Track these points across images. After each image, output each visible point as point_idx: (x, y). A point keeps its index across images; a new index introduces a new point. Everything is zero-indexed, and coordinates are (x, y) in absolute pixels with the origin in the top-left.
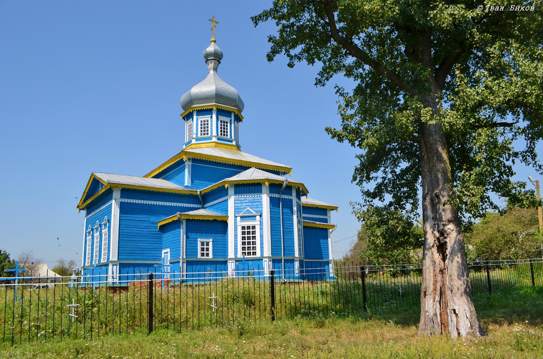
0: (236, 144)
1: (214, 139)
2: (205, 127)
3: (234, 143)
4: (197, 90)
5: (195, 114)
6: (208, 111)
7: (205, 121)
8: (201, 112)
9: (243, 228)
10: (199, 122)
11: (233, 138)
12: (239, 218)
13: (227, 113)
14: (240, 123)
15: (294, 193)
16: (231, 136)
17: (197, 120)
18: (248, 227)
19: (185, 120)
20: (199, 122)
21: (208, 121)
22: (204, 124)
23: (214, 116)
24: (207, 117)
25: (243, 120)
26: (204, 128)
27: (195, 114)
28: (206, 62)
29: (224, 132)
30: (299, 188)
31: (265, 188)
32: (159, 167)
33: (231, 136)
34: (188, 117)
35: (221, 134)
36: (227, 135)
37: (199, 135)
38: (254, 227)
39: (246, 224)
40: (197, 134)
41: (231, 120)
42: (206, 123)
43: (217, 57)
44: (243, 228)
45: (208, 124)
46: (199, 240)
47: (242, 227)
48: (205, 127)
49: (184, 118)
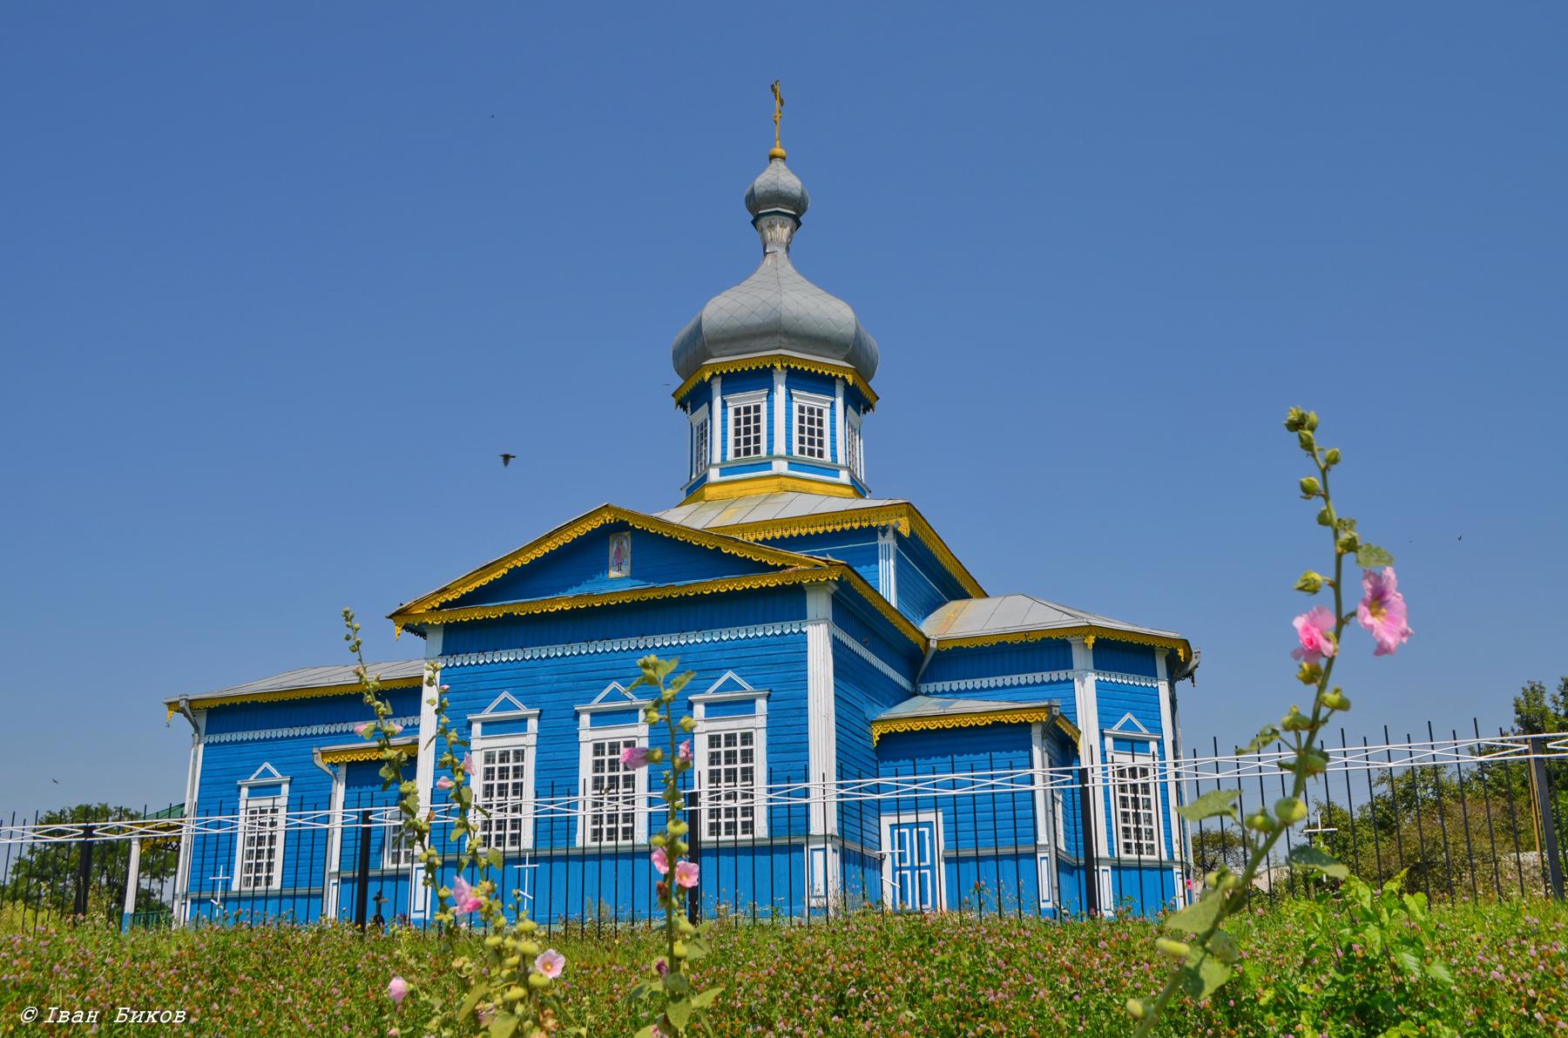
1: (780, 467)
2: (748, 423)
3: (844, 477)
4: (725, 308)
5: (717, 387)
6: (759, 378)
8: (736, 381)
10: (731, 412)
11: (841, 460)
12: (1109, 741)
13: (821, 383)
16: (834, 455)
17: (724, 405)
19: (685, 409)
20: (731, 412)
21: (757, 409)
23: (781, 391)
24: (755, 398)
25: (877, 405)
27: (717, 387)
28: (754, 223)
30: (1174, 652)
31: (1081, 657)
32: (537, 544)
33: (834, 455)
34: (695, 398)
35: (802, 451)
36: (821, 454)
37: (730, 456)
38: (747, 738)
39: (723, 726)
41: (833, 404)
42: (752, 415)
43: (794, 208)
45: (757, 419)
47: (712, 738)
48: (748, 423)
49: (682, 404)
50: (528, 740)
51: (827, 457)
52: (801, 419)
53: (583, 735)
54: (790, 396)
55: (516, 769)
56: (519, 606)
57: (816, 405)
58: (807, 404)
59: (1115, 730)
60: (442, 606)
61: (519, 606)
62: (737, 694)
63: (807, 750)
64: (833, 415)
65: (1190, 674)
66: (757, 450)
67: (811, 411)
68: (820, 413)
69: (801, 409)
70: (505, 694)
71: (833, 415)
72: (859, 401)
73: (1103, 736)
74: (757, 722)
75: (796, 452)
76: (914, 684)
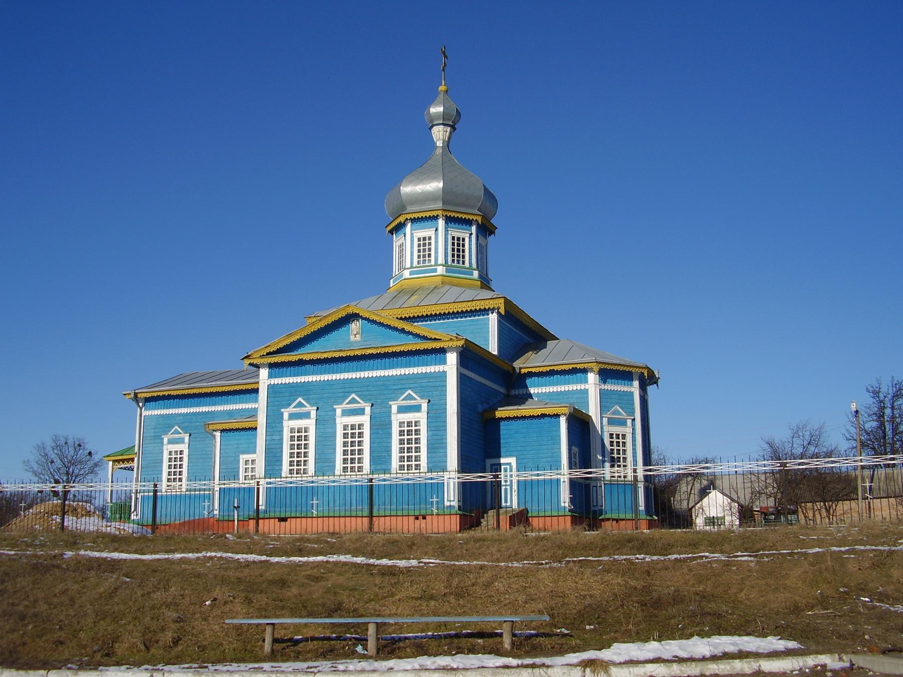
0: (480, 276)
2: (424, 242)
7: (424, 239)
9: (292, 430)
12: (605, 420)
14: (491, 238)
15: (636, 383)
16: (470, 263)
18: (409, 424)
21: (430, 238)
22: (424, 245)
24: (428, 232)
26: (424, 250)
29: (458, 250)
35: (453, 261)
37: (415, 264)
40: (412, 263)
42: (427, 242)
44: (292, 430)
45: (430, 244)
46: (241, 456)
48: (424, 242)
50: (365, 420)
51: (467, 264)
52: (453, 244)
53: (393, 417)
54: (446, 231)
55: (359, 433)
56: (407, 327)
57: (461, 235)
58: (456, 235)
59: (609, 415)
60: (268, 354)
61: (407, 327)
62: (412, 403)
63: (446, 430)
64: (470, 241)
65: (656, 383)
66: (430, 261)
67: (458, 239)
68: (464, 240)
69: (453, 238)
70: (300, 399)
71: (470, 241)
72: (486, 230)
73: (602, 418)
74: (422, 417)
75: (450, 262)
76: (508, 389)
